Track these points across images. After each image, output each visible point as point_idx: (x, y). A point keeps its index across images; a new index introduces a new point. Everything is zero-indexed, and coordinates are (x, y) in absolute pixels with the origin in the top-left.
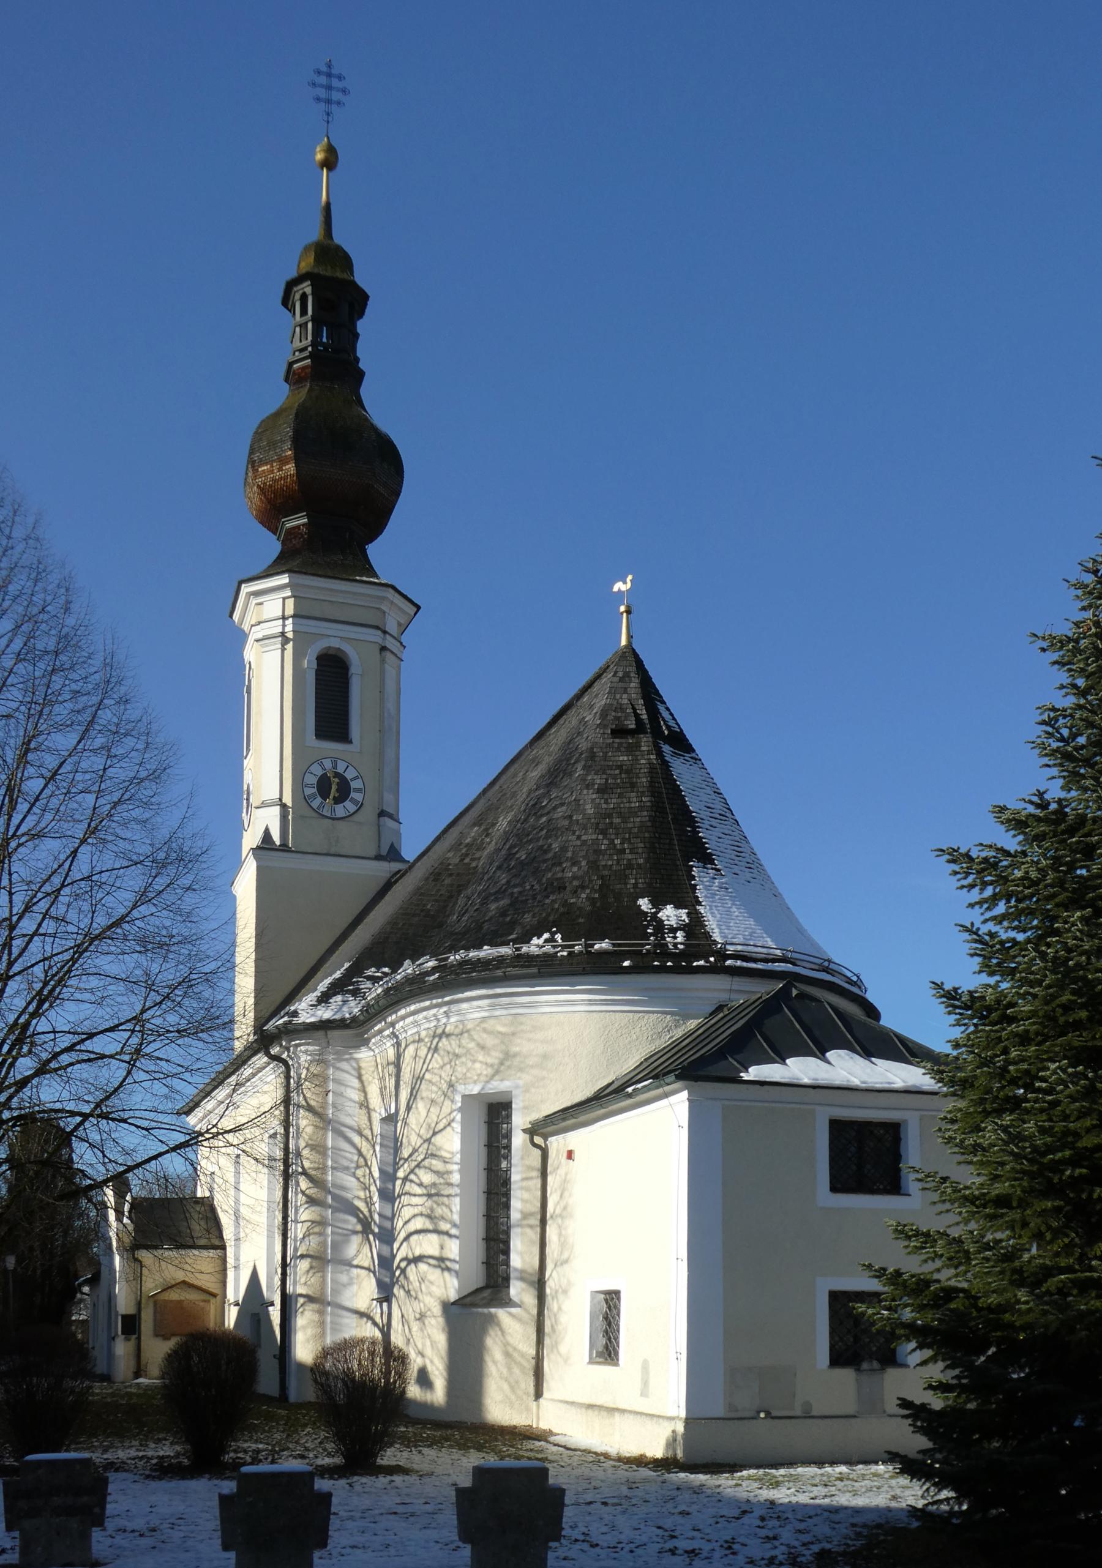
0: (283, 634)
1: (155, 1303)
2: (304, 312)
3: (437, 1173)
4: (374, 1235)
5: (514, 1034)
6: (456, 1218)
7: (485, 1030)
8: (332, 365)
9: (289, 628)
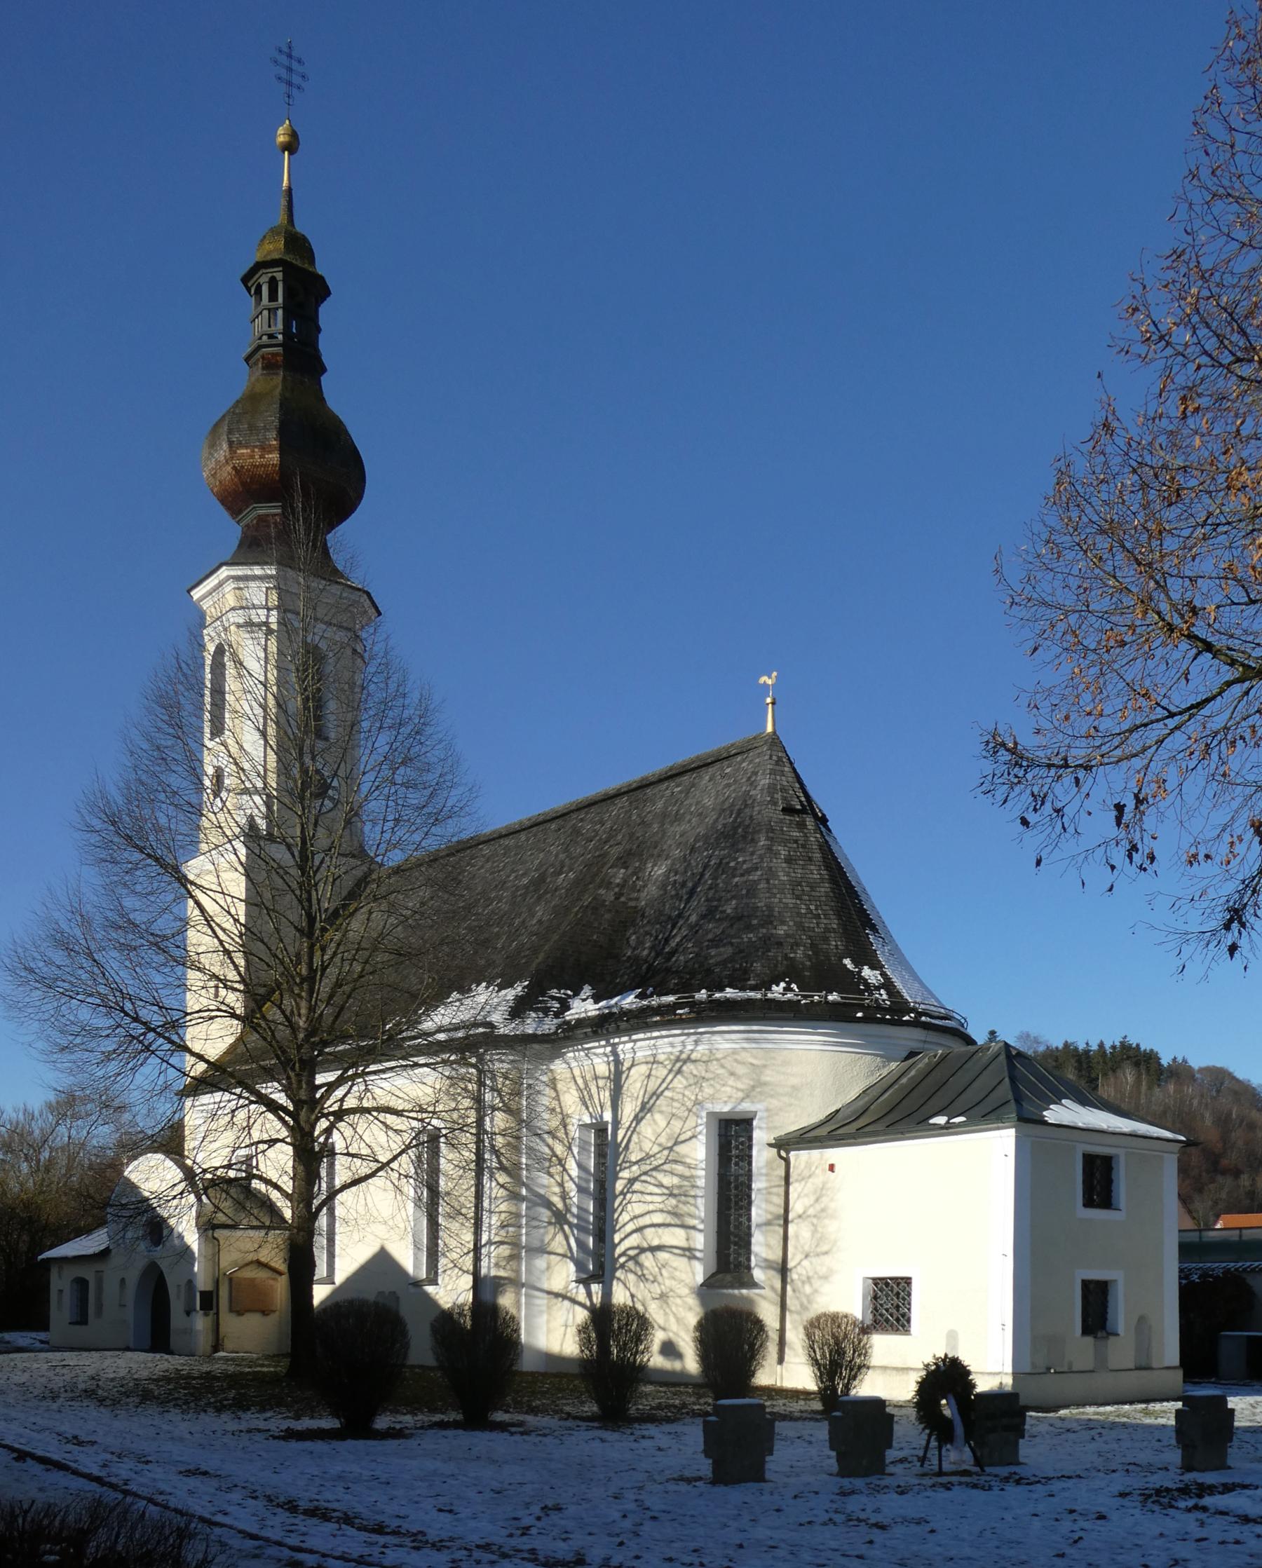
0: (266, 624)
1: (231, 1280)
2: (273, 297)
3: (681, 1176)
4: (571, 1225)
5: (765, 1066)
6: (703, 1214)
7: (736, 1060)
8: (298, 357)
9: (273, 619)
